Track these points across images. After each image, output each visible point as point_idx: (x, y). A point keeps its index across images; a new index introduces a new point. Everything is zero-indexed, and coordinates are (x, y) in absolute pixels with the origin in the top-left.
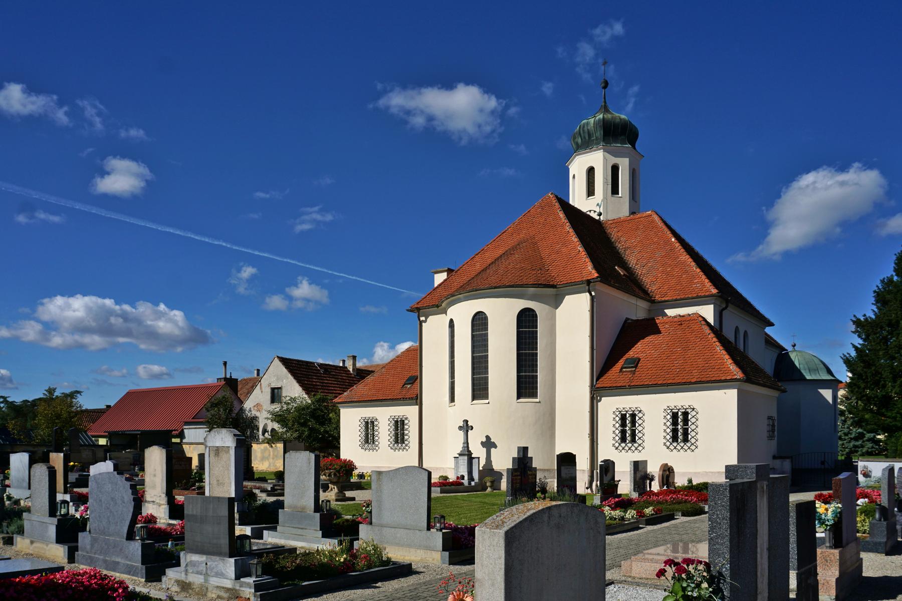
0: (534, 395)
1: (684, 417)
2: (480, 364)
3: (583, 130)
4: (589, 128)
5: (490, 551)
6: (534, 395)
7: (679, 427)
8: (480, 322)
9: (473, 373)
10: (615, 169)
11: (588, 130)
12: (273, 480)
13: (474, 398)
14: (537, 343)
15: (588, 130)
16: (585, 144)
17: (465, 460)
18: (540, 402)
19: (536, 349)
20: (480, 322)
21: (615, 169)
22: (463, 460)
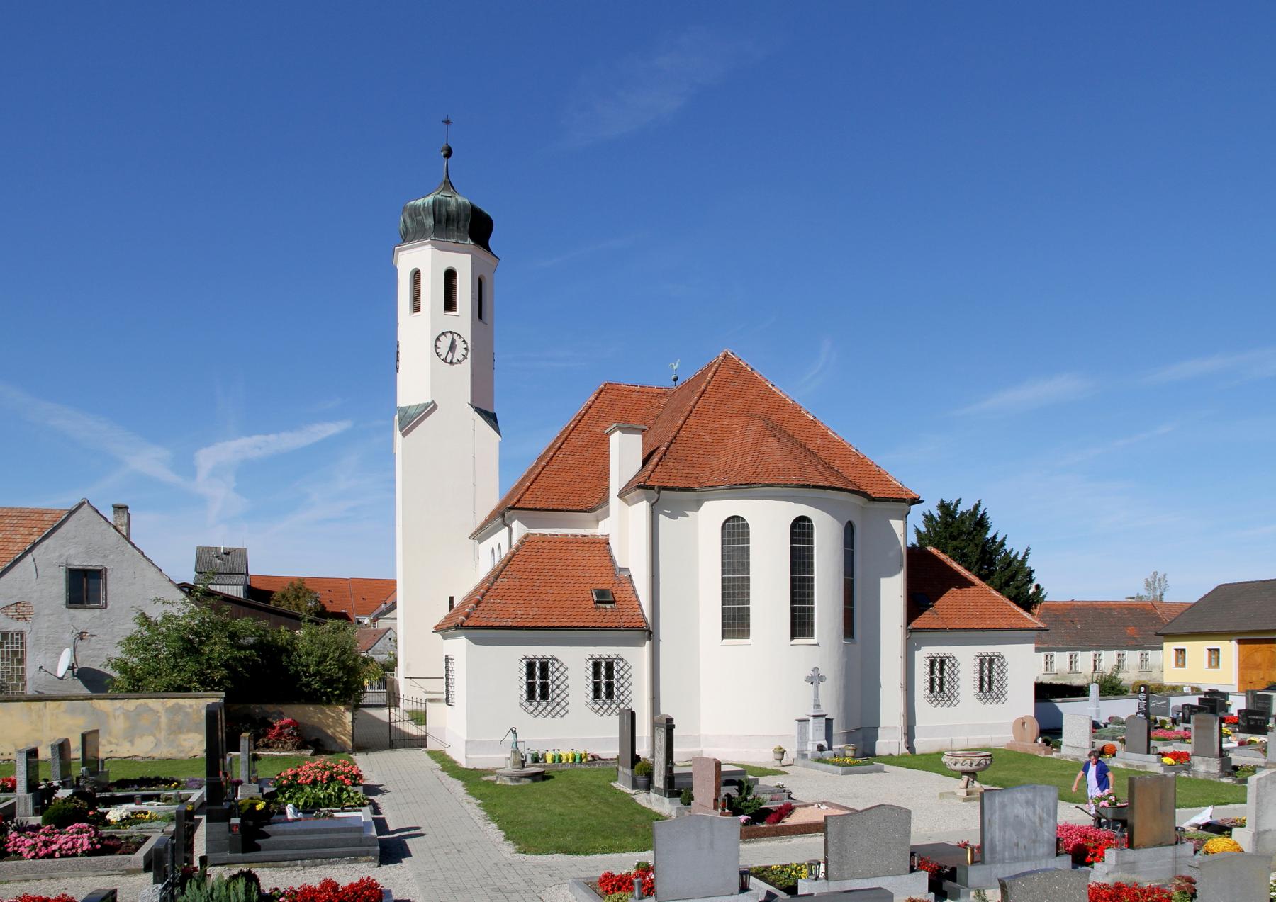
0: (809, 634)
1: (594, 669)
2: (801, 590)
3: (440, 211)
4: (449, 209)
5: (511, 830)
6: (809, 634)
7: (604, 681)
8: (735, 531)
9: (793, 601)
10: (450, 276)
11: (447, 211)
12: (910, 733)
13: (794, 634)
14: (812, 564)
15: (447, 211)
16: (411, 235)
17: (822, 723)
18: (818, 645)
19: (812, 572)
20: (735, 531)
21: (450, 276)
22: (819, 723)
